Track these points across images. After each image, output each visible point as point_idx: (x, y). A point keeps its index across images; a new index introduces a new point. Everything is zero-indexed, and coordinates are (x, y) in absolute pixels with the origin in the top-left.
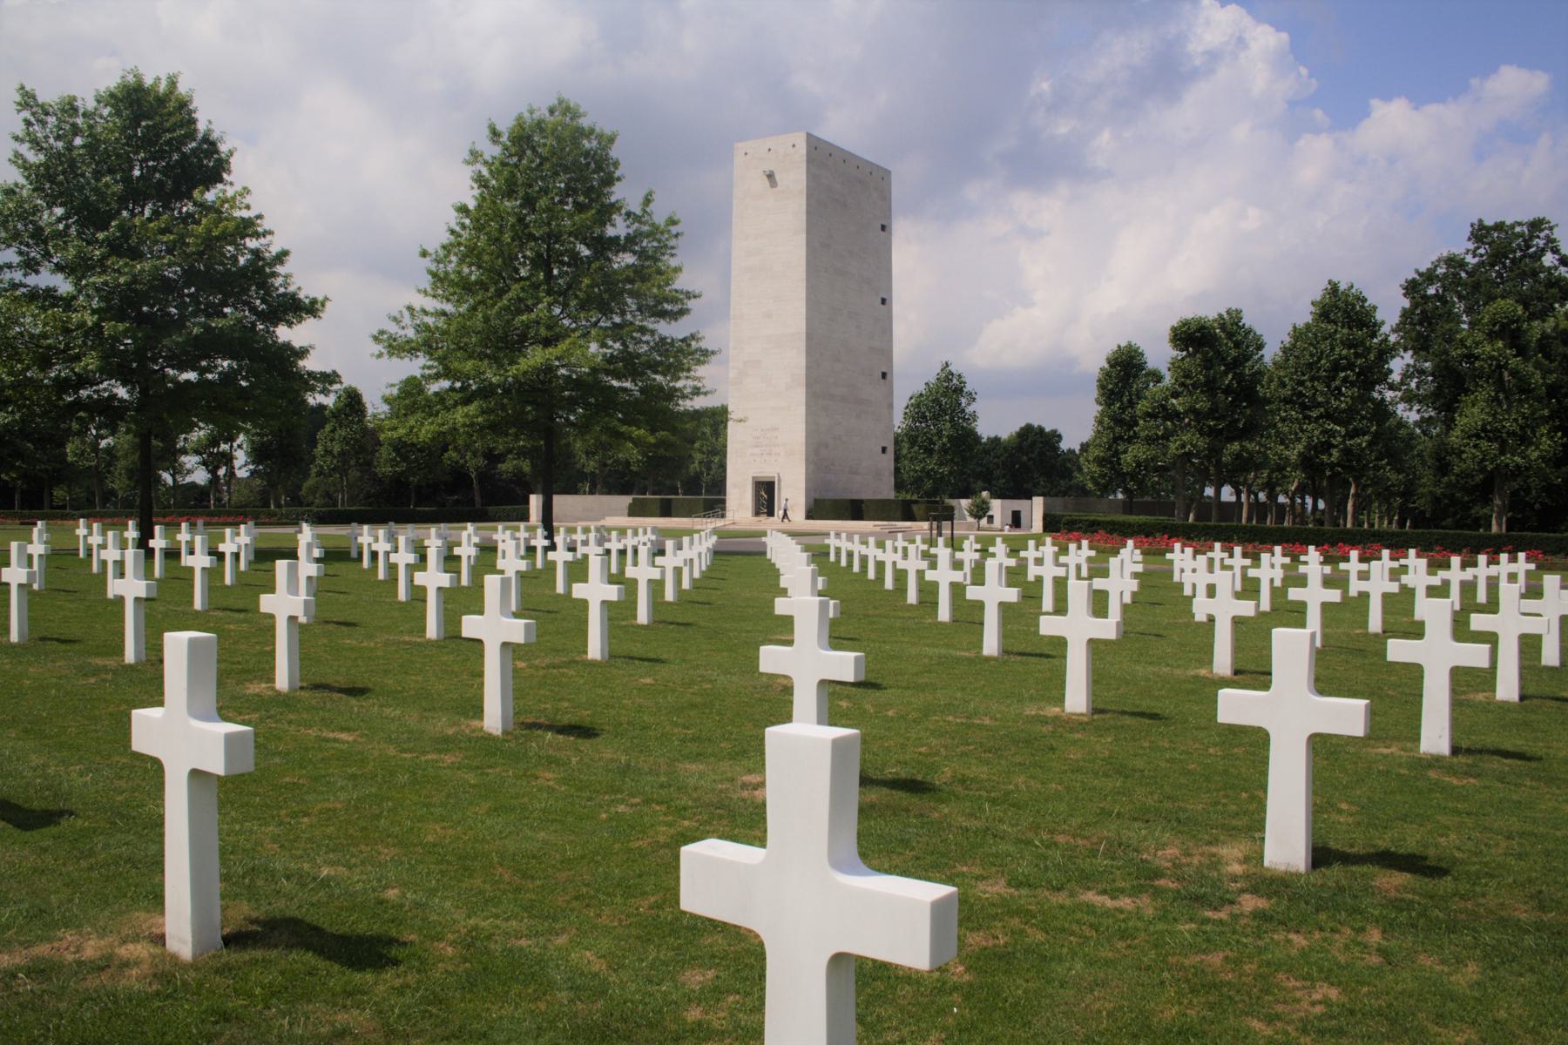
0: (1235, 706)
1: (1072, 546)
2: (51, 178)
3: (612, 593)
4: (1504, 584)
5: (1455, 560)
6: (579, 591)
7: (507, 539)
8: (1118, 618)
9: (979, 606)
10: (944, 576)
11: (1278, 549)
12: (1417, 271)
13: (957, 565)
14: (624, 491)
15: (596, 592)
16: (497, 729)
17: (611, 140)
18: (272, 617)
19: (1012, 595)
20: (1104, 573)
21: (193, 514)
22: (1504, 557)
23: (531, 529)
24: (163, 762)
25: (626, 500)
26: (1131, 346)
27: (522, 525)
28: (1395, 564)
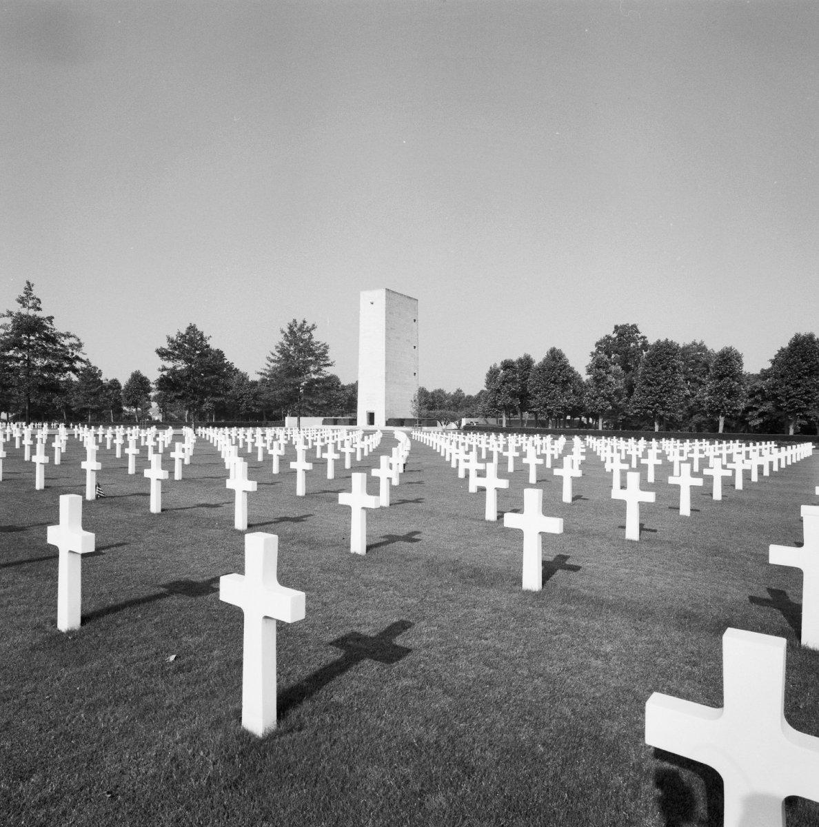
0: (617, 493)
1: (468, 434)
2: (21, 319)
3: (337, 456)
4: (763, 450)
5: (717, 442)
6: (325, 456)
7: (280, 432)
8: (497, 463)
9: (272, 456)
10: (260, 444)
11: (773, 442)
12: (162, 353)
13: (265, 441)
14: (319, 415)
15: (330, 456)
16: (267, 542)
17: (179, 333)
18: (85, 470)
19: (517, 454)
20: (554, 444)
21: (747, 439)
22: (751, 444)
23: (287, 429)
24: (279, 585)
25: (322, 419)
26: (246, 375)
27: (284, 428)
28: (691, 444)
